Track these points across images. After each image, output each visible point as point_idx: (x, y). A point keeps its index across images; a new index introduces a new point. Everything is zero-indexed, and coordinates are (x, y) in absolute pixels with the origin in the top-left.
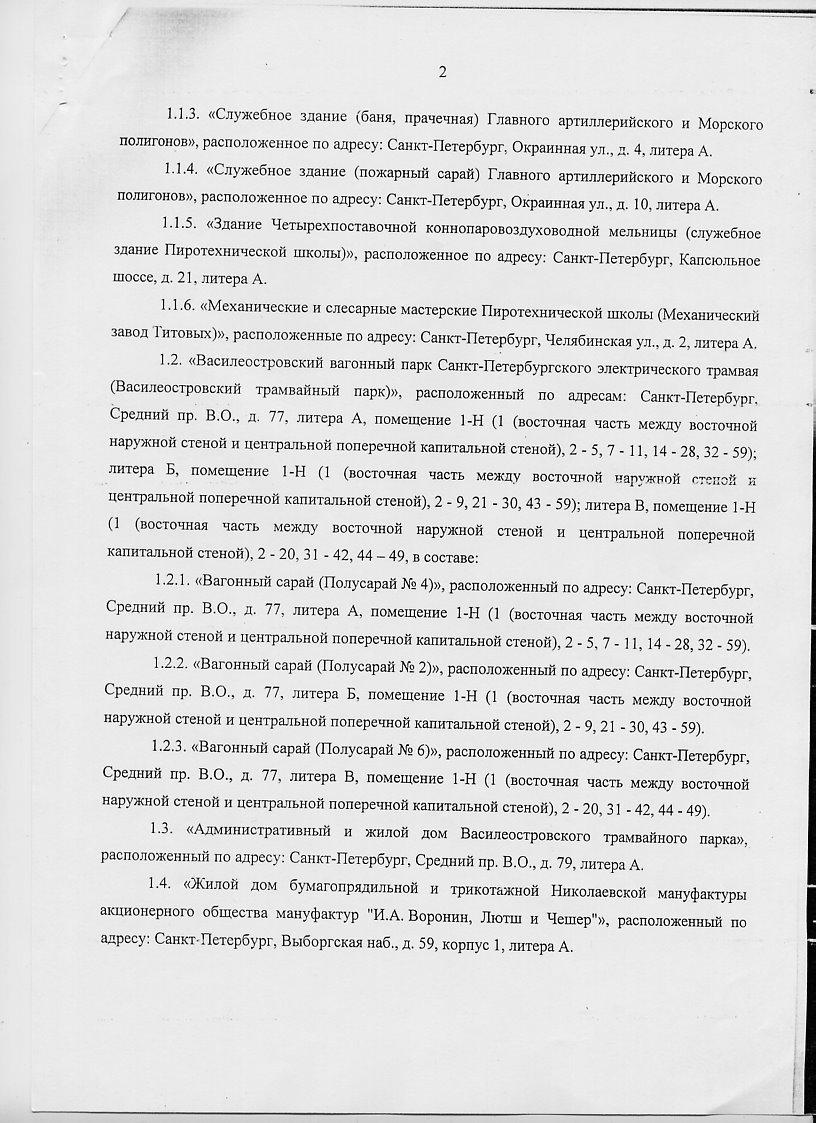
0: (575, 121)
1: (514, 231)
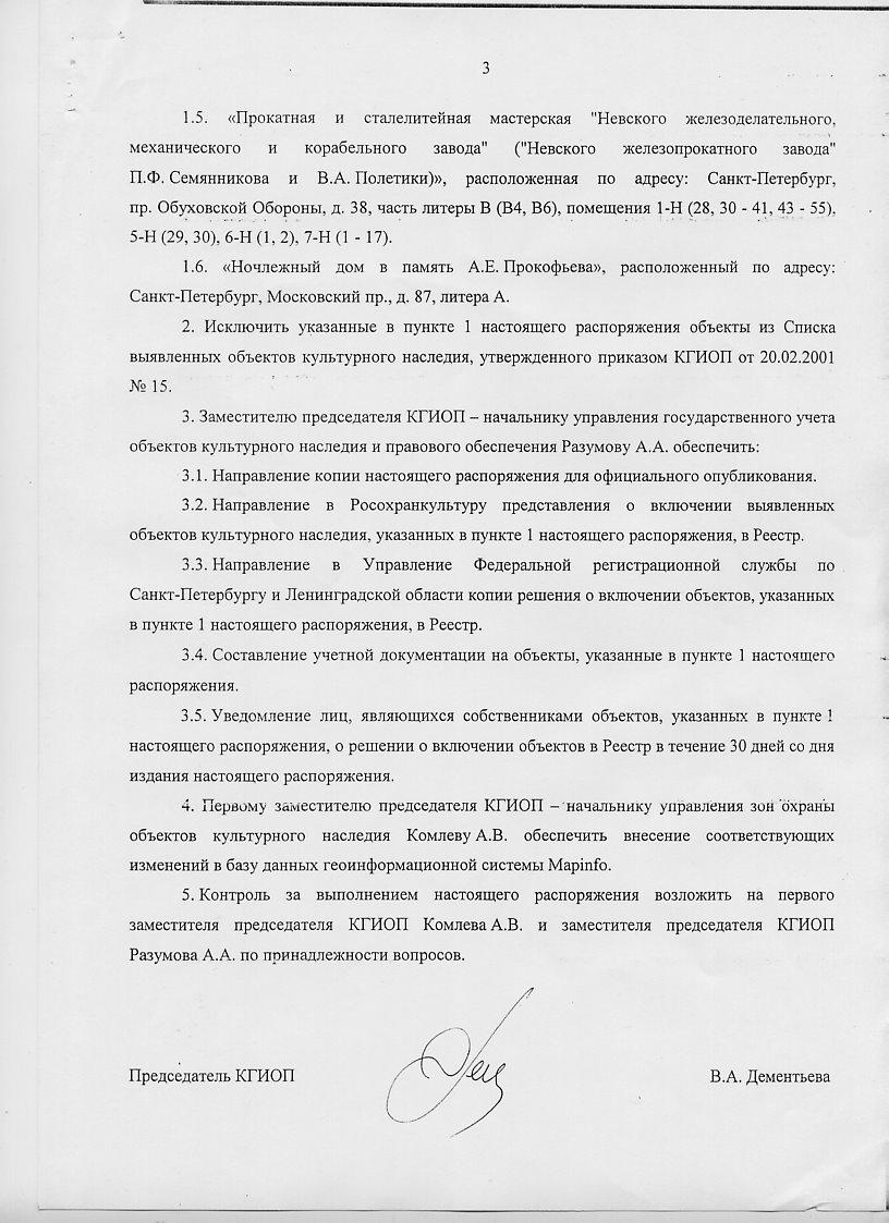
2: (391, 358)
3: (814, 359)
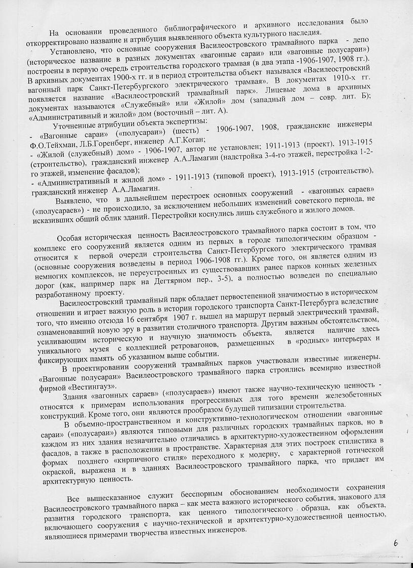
1: (87, 462)
3: (328, 58)
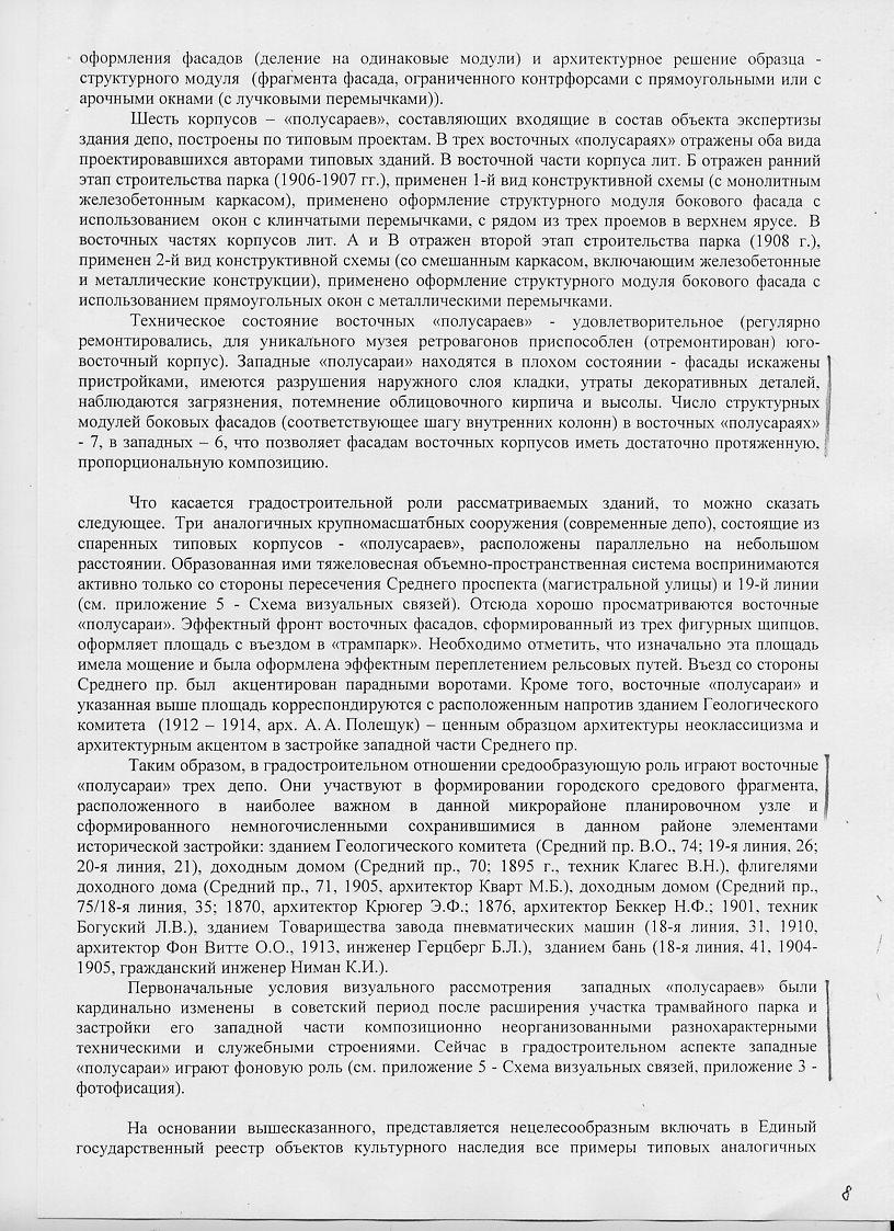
0: (787, 121)
2: (195, 807)
